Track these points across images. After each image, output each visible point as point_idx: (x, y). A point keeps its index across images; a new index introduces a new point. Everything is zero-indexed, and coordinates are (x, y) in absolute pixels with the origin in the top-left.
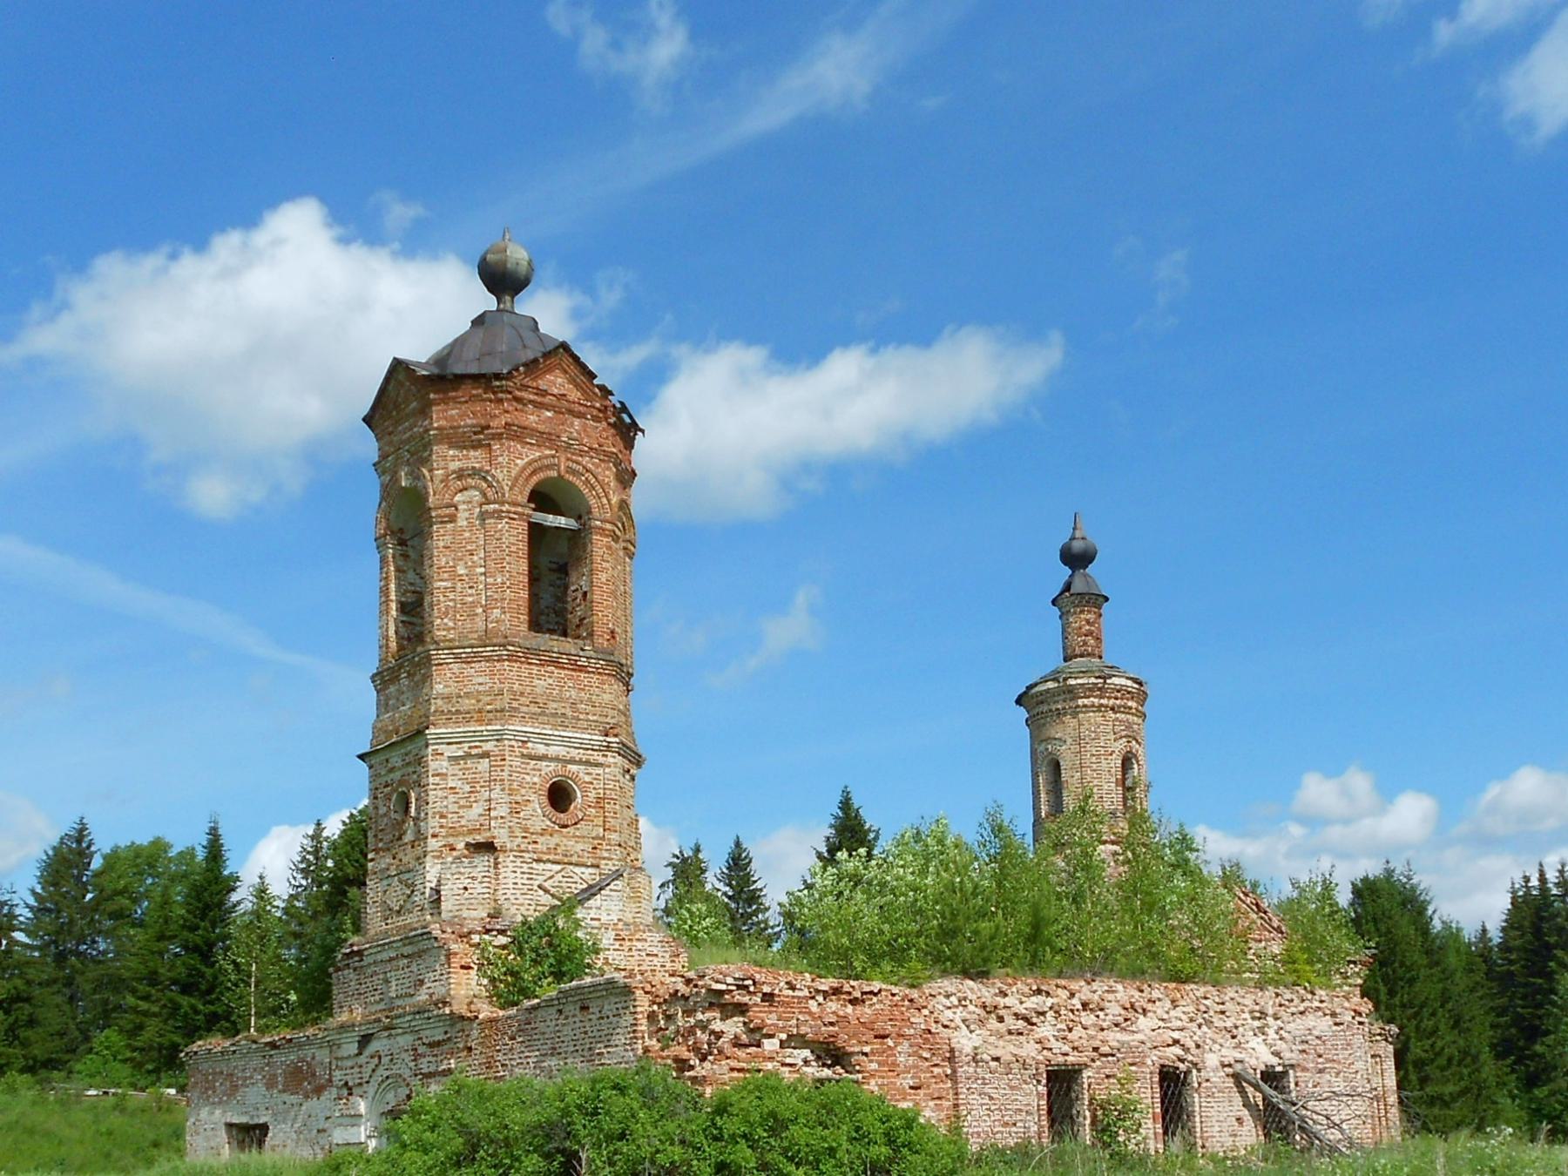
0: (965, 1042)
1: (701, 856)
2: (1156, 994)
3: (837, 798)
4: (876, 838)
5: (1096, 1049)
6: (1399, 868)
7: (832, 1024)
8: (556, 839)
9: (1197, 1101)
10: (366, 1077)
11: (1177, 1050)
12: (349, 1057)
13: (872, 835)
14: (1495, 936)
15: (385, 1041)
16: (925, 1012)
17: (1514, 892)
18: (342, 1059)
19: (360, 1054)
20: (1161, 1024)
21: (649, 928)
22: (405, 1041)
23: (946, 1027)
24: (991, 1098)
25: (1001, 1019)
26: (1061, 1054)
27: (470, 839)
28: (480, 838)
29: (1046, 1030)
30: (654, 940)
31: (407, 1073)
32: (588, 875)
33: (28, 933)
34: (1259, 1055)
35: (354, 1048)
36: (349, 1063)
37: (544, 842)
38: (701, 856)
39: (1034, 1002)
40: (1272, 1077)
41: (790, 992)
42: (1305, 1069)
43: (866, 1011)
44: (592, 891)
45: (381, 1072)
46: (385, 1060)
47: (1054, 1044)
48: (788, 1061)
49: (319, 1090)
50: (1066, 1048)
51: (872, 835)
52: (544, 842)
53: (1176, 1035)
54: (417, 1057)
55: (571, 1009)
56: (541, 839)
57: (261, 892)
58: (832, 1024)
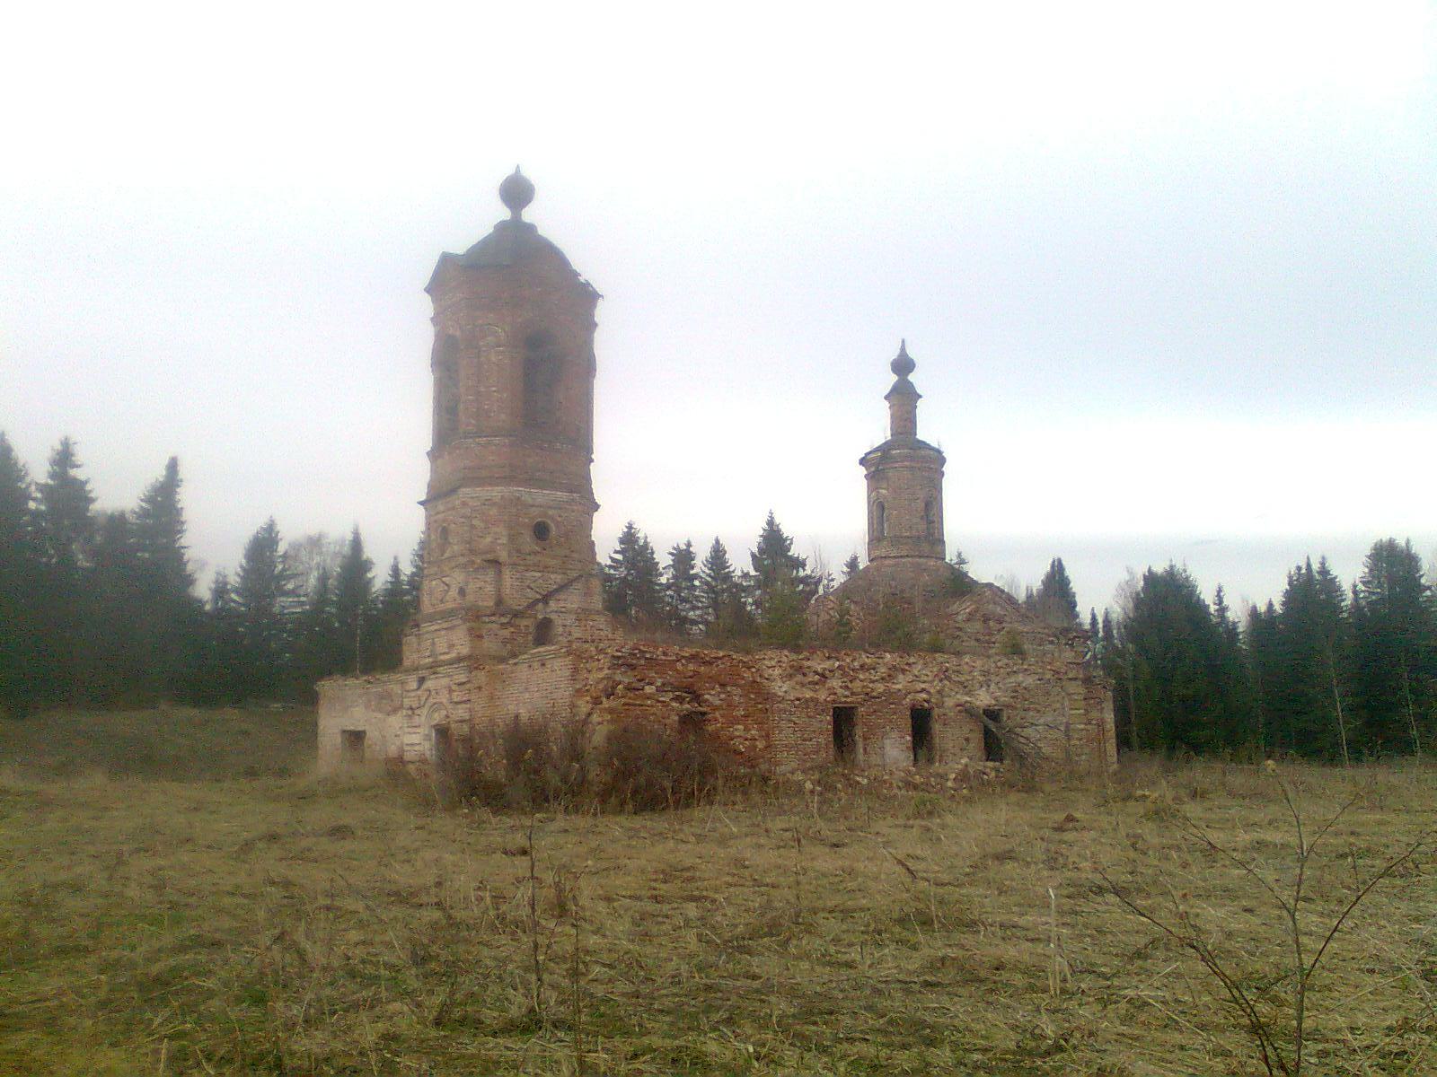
0: (781, 688)
1: (691, 549)
2: (912, 660)
3: (766, 518)
4: (791, 543)
5: (867, 694)
6: (1179, 566)
7: (691, 677)
8: (538, 558)
9: (937, 727)
10: (422, 703)
11: (924, 696)
12: (413, 690)
13: (788, 542)
14: (1278, 608)
15: (433, 682)
16: (754, 670)
17: (1290, 577)
18: (408, 691)
19: (418, 688)
20: (915, 678)
21: (598, 613)
22: (444, 681)
23: (767, 679)
24: (795, 724)
25: (804, 675)
26: (844, 697)
27: (484, 557)
28: (489, 557)
29: (835, 683)
30: (601, 621)
31: (444, 701)
32: (557, 578)
33: (238, 593)
34: (983, 699)
35: (414, 685)
36: (413, 694)
37: (531, 559)
38: (691, 549)
39: (827, 664)
40: (992, 714)
41: (663, 658)
42: (1014, 708)
43: (715, 670)
44: (562, 588)
45: (432, 701)
46: (433, 693)
47: (840, 691)
48: (661, 699)
49: (395, 711)
50: (847, 693)
51: (788, 542)
52: (531, 559)
53: (923, 686)
54: (451, 691)
55: (536, 665)
56: (528, 557)
57: (396, 571)
58: (691, 677)
